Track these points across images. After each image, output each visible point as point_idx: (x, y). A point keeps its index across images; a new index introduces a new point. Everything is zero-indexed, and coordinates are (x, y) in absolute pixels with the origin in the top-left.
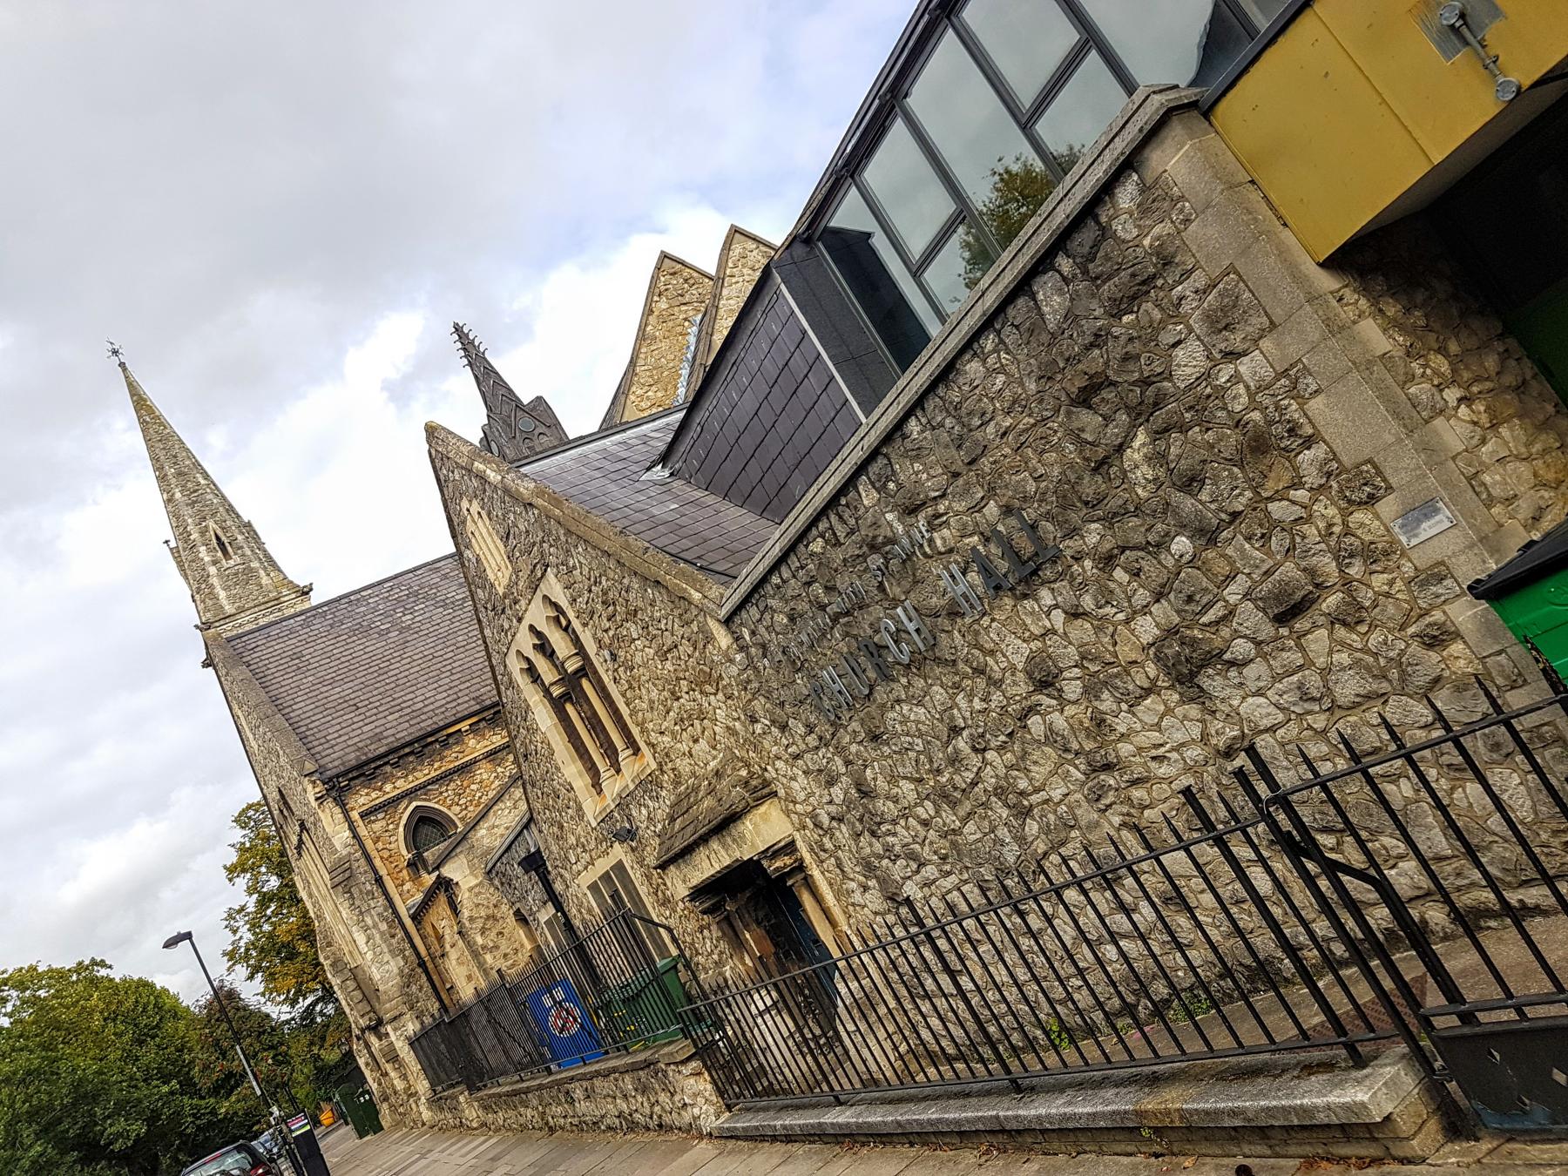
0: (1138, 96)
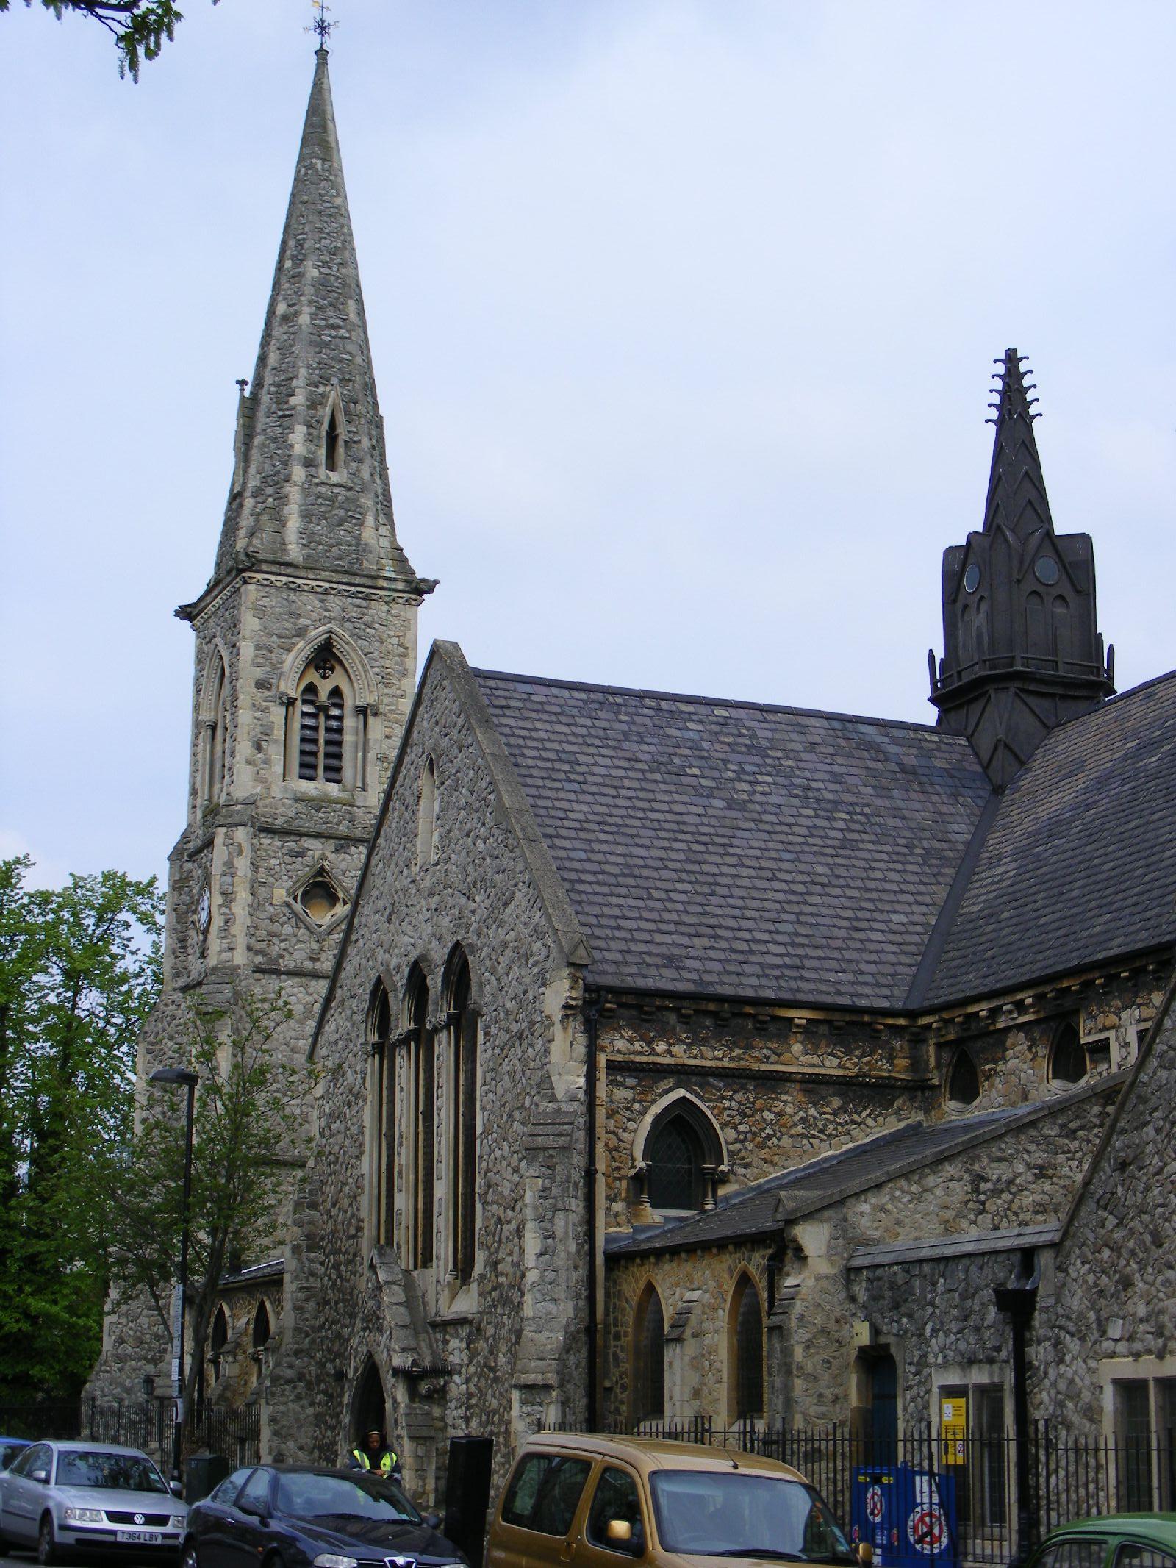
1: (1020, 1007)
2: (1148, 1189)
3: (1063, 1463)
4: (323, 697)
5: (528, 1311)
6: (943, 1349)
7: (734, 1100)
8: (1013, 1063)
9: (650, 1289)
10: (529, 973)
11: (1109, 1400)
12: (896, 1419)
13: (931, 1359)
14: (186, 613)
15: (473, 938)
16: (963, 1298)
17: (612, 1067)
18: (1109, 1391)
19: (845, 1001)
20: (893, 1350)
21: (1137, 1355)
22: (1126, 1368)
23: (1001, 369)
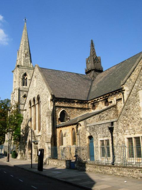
0: (25, 71)
1: (101, 98)
2: (131, 112)
3: (119, 149)
5: (47, 134)
6: (100, 136)
7: (69, 110)
8: (100, 105)
9: (61, 131)
10: (46, 96)
11: (126, 141)
12: (93, 144)
13: (98, 137)
15: (40, 94)
16: (103, 129)
19: (81, 99)
20: (93, 136)
21: (130, 134)
23: (91, 42)
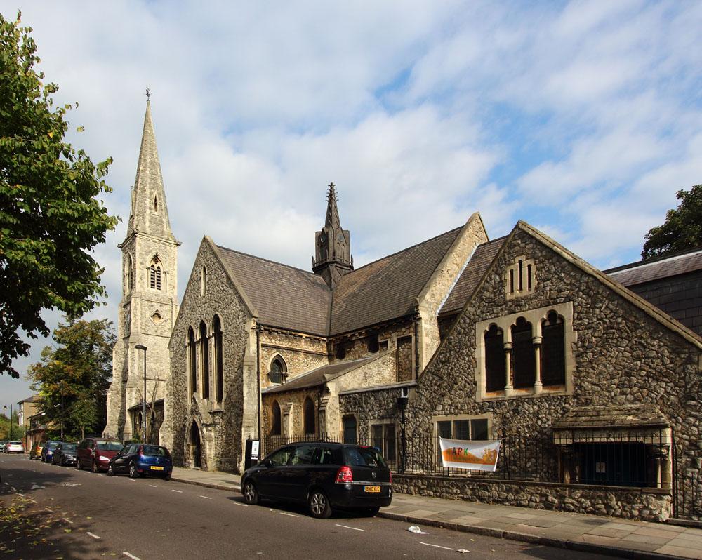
1: (360, 334)
4: (156, 269)
14: (120, 246)
17: (263, 345)
18: (436, 425)
21: (446, 414)
22: (443, 418)
